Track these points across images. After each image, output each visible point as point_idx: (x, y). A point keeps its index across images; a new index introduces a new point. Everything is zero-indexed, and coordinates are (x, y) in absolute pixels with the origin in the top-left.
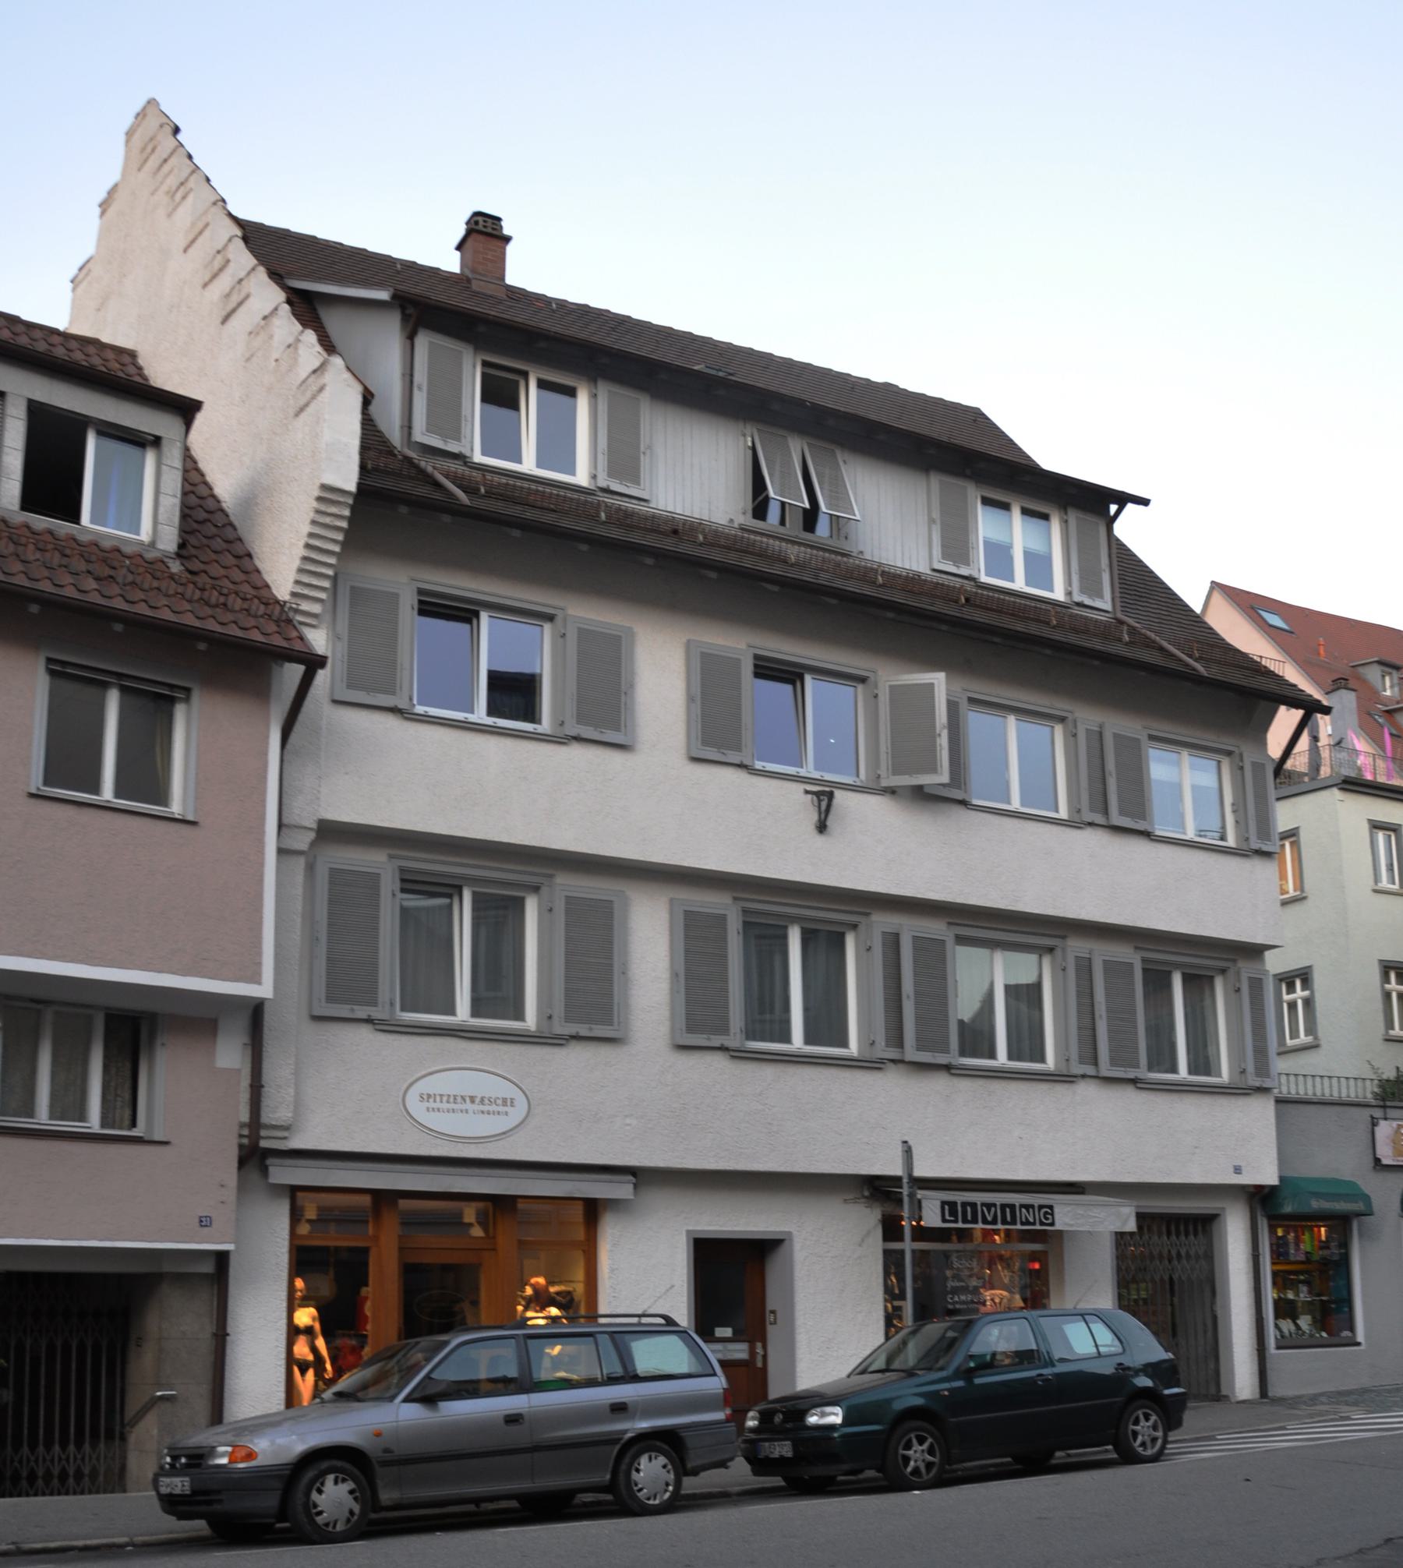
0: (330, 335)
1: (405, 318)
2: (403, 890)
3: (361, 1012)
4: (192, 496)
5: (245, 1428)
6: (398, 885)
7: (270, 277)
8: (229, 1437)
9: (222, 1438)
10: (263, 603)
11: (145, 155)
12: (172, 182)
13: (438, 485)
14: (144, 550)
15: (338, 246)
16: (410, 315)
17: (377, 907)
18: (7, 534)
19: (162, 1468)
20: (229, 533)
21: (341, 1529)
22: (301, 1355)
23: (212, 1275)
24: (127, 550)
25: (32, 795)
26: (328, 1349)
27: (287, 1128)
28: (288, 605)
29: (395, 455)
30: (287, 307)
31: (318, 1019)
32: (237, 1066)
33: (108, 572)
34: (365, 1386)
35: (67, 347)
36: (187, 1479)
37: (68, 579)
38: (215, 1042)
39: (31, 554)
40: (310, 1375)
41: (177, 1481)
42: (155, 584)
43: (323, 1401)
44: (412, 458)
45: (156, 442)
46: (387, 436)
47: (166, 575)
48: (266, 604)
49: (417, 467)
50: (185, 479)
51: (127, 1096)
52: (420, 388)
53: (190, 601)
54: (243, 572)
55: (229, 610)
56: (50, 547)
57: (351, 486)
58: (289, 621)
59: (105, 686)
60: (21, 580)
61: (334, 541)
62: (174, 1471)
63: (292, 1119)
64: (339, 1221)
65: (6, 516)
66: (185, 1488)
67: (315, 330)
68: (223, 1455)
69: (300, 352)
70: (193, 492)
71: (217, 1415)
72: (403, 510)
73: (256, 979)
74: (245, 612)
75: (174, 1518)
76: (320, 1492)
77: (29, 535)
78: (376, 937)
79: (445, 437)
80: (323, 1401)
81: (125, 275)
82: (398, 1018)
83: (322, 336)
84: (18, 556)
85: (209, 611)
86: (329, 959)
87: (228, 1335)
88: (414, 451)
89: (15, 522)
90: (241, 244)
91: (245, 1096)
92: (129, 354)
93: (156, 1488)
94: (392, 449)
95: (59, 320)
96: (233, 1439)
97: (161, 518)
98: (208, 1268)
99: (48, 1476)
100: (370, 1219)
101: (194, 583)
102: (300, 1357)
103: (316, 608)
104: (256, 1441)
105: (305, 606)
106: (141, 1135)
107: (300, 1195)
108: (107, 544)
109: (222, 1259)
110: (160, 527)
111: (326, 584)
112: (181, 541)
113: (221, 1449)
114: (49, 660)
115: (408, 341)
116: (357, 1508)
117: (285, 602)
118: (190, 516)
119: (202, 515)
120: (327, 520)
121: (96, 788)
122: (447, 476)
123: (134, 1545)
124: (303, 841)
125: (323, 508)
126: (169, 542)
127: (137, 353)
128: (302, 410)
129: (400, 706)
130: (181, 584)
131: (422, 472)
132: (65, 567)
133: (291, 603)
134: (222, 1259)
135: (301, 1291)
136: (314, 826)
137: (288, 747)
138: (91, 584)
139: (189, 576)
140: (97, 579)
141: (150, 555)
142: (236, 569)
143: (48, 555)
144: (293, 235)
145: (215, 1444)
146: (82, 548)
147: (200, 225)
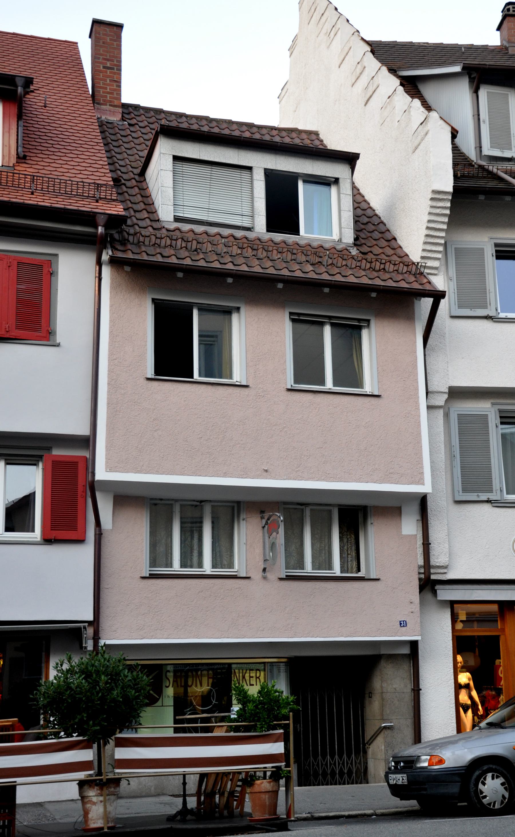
0: (427, 100)
1: (471, 81)
2: (502, 423)
3: (484, 497)
4: (358, 209)
5: (437, 745)
6: (499, 420)
7: (389, 72)
8: (428, 750)
9: (424, 751)
10: (406, 265)
11: (311, 14)
12: (328, 27)
13: (501, 180)
14: (335, 244)
15: (425, 45)
16: (474, 78)
17: (488, 434)
18: (262, 246)
19: (390, 769)
20: (381, 227)
21: (499, 807)
22: (464, 701)
23: (409, 654)
24: (327, 246)
25: (289, 390)
26: (479, 697)
27: (446, 567)
28: (420, 264)
29: (473, 166)
30: (401, 88)
31: (458, 502)
32: (414, 532)
33: (318, 260)
34: (503, 720)
35: (281, 136)
36: (405, 775)
37: (296, 267)
38: (401, 520)
39: (275, 255)
40: (470, 712)
41: (399, 776)
42: (344, 263)
43: (480, 729)
44: (484, 166)
45: (336, 181)
46: (467, 154)
47: (349, 257)
48: (408, 266)
49: (488, 171)
50: (354, 201)
51: (354, 554)
52: (484, 122)
53: (364, 270)
54: (392, 249)
55: (386, 272)
56: (245, 245)
57: (450, 189)
58: (422, 274)
59: (322, 324)
60: (271, 271)
61: (443, 223)
62: (397, 771)
63: (448, 562)
64: (479, 621)
65: (259, 236)
66: (404, 781)
67: (419, 99)
68: (425, 761)
69: (412, 113)
70: (359, 207)
71: (417, 738)
72: (482, 197)
73: (421, 481)
74: (396, 272)
75: (399, 799)
76: (484, 784)
77: (274, 245)
78: (489, 452)
79: (502, 149)
80: (480, 729)
81: (307, 88)
82: (505, 499)
83: (427, 107)
84: (268, 257)
85: (376, 274)
86: (462, 468)
87: (421, 690)
88: (484, 161)
89: (278, 241)
90: (371, 55)
91: (420, 550)
92: (315, 134)
93: (388, 782)
94: (471, 162)
95: (274, 122)
96: (430, 751)
97: (343, 225)
98: (406, 651)
99: (325, 774)
100: (499, 619)
101: (366, 260)
102: (462, 702)
103: (436, 264)
104: (444, 752)
105: (430, 263)
106: (364, 576)
107: (455, 606)
108: (315, 244)
109: (414, 645)
110: (343, 229)
111: (441, 249)
112: (355, 236)
113: (423, 758)
114: (291, 314)
115: (475, 95)
116: (507, 795)
117: (418, 263)
118: (359, 221)
119: (365, 220)
120: (438, 211)
121: (322, 382)
122: (506, 173)
123: (376, 815)
124: (440, 400)
125: (435, 204)
126: (349, 238)
127: (319, 133)
128: (416, 148)
129: (491, 315)
130: (359, 261)
131: (490, 173)
132: (294, 260)
133: (422, 263)
134: (414, 645)
135: (461, 663)
136: (447, 391)
137: (428, 346)
138: (309, 268)
139: (362, 256)
140: (312, 265)
141: (339, 247)
142: (388, 248)
143: (284, 254)
144: (399, 44)
145: (420, 755)
146: (303, 248)
147: (347, 49)
